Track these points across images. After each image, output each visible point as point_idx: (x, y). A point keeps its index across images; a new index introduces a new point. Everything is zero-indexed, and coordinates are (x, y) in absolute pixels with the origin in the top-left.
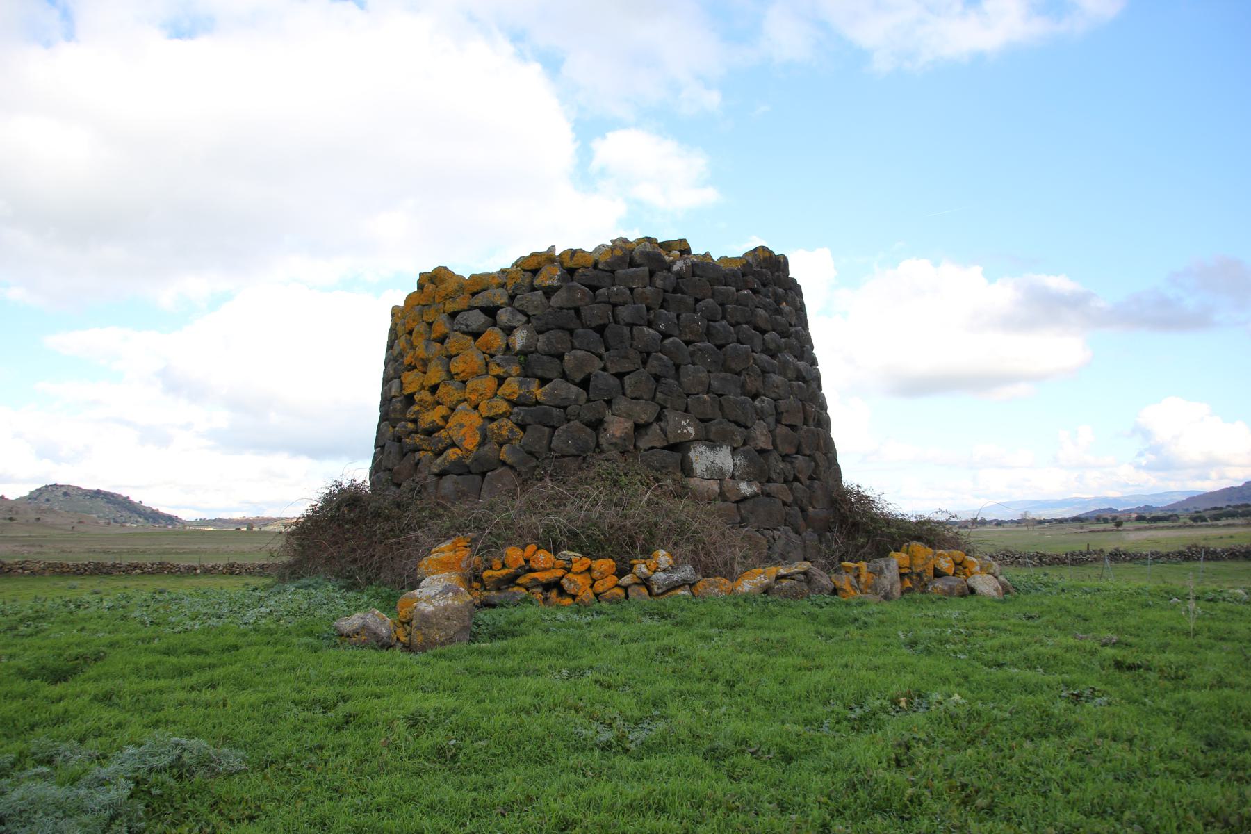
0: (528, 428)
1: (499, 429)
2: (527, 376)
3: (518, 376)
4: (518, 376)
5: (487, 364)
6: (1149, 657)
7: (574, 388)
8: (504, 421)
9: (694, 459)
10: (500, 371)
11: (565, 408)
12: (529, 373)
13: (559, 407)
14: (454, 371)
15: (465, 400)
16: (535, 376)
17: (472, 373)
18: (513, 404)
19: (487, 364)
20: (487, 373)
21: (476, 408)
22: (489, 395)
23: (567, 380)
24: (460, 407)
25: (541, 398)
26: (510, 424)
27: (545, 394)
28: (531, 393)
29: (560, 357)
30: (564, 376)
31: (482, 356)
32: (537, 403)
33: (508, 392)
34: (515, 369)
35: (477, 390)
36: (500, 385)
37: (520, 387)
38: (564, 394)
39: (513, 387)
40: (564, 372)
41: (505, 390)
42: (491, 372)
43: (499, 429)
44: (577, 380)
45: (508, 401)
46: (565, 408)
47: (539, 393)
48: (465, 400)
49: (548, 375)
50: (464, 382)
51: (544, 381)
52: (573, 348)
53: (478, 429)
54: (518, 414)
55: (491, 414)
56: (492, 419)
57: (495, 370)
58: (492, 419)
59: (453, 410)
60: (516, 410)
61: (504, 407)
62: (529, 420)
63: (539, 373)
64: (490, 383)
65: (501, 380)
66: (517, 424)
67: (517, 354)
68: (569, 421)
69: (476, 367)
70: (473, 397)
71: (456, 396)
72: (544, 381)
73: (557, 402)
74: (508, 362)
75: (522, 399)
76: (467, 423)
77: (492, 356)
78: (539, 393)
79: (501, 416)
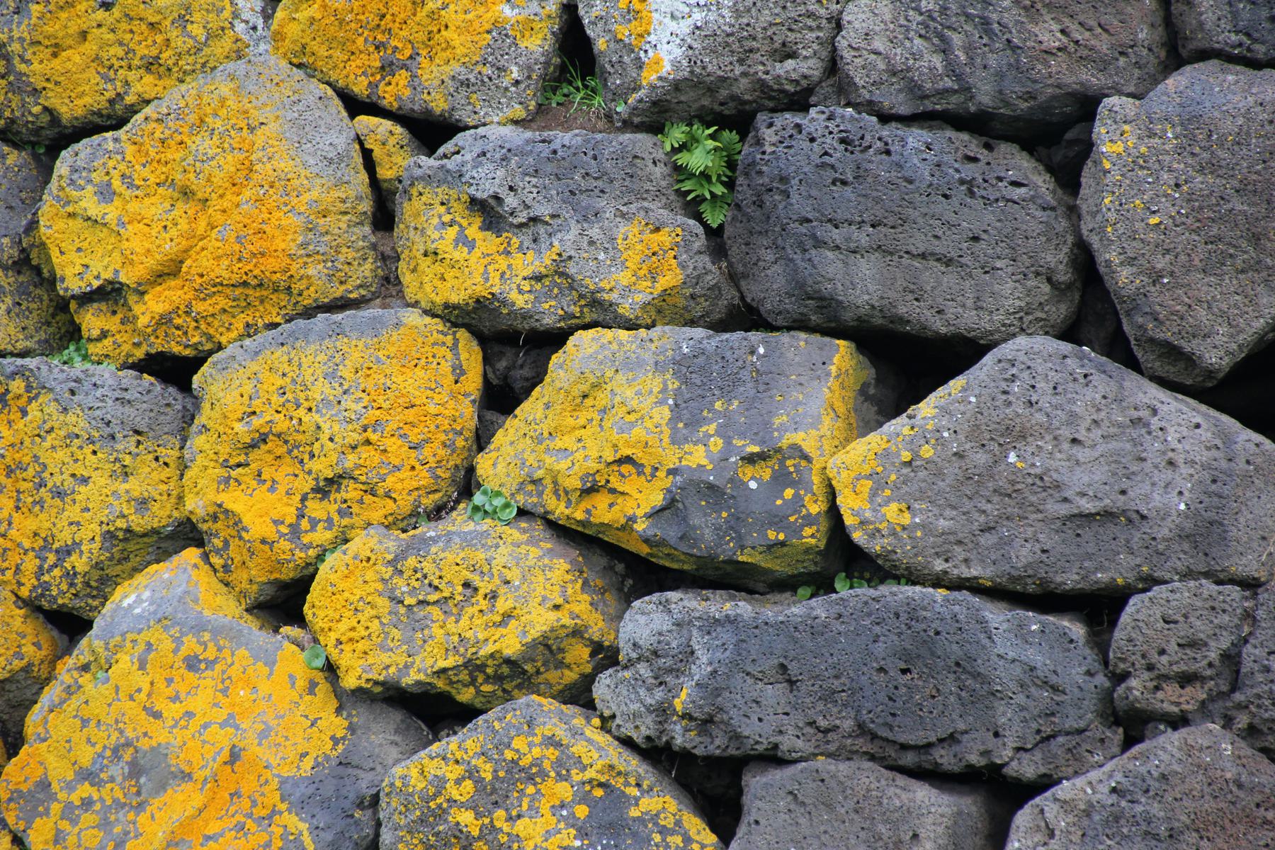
0: (760, 789)
1: (492, 795)
2: (746, 317)
3: (665, 311)
4: (665, 311)
5: (384, 215)
6: (1098, 44)
7: (1187, 426)
8: (534, 727)
9: (1083, 184)
10: (505, 273)
11: (1099, 608)
12: (770, 286)
13: (1048, 600)
14: (76, 269)
15: (187, 534)
16: (828, 321)
17: (250, 289)
18: (632, 571)
19: (384, 215)
20: (388, 286)
21: (284, 603)
22: (409, 483)
23: (1120, 351)
24: (132, 598)
25: (876, 518)
26: (596, 751)
27: (909, 477)
28: (785, 464)
29: (1057, 136)
30: (1092, 313)
31: (338, 131)
32: (845, 557)
33: (579, 454)
34: (641, 253)
35: (295, 448)
36: (500, 399)
37: (686, 418)
38: (1086, 481)
39: (615, 418)
40: (1086, 269)
41: (548, 441)
42: (425, 283)
43: (492, 795)
44: (1217, 352)
45: (577, 538)
46: (1099, 608)
47: (847, 457)
48: (187, 534)
49: (943, 306)
50: (175, 371)
51: (906, 363)
52: (1177, 51)
53: (306, 796)
54: (667, 663)
55: (420, 665)
56: (432, 710)
57: (457, 260)
58: (432, 710)
59: (69, 625)
60: (646, 621)
61: (541, 594)
62: (762, 716)
63: (864, 284)
64: (416, 376)
65: (512, 355)
66: (657, 754)
67: (654, 119)
68: (1133, 726)
69: (285, 234)
70: (261, 509)
71: (102, 497)
72: (906, 363)
73: (1025, 551)
74: (579, 186)
75: (707, 531)
76: (199, 749)
77: (430, 131)
78: (847, 457)
79: (514, 675)
